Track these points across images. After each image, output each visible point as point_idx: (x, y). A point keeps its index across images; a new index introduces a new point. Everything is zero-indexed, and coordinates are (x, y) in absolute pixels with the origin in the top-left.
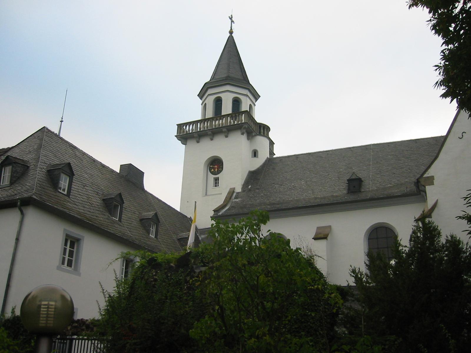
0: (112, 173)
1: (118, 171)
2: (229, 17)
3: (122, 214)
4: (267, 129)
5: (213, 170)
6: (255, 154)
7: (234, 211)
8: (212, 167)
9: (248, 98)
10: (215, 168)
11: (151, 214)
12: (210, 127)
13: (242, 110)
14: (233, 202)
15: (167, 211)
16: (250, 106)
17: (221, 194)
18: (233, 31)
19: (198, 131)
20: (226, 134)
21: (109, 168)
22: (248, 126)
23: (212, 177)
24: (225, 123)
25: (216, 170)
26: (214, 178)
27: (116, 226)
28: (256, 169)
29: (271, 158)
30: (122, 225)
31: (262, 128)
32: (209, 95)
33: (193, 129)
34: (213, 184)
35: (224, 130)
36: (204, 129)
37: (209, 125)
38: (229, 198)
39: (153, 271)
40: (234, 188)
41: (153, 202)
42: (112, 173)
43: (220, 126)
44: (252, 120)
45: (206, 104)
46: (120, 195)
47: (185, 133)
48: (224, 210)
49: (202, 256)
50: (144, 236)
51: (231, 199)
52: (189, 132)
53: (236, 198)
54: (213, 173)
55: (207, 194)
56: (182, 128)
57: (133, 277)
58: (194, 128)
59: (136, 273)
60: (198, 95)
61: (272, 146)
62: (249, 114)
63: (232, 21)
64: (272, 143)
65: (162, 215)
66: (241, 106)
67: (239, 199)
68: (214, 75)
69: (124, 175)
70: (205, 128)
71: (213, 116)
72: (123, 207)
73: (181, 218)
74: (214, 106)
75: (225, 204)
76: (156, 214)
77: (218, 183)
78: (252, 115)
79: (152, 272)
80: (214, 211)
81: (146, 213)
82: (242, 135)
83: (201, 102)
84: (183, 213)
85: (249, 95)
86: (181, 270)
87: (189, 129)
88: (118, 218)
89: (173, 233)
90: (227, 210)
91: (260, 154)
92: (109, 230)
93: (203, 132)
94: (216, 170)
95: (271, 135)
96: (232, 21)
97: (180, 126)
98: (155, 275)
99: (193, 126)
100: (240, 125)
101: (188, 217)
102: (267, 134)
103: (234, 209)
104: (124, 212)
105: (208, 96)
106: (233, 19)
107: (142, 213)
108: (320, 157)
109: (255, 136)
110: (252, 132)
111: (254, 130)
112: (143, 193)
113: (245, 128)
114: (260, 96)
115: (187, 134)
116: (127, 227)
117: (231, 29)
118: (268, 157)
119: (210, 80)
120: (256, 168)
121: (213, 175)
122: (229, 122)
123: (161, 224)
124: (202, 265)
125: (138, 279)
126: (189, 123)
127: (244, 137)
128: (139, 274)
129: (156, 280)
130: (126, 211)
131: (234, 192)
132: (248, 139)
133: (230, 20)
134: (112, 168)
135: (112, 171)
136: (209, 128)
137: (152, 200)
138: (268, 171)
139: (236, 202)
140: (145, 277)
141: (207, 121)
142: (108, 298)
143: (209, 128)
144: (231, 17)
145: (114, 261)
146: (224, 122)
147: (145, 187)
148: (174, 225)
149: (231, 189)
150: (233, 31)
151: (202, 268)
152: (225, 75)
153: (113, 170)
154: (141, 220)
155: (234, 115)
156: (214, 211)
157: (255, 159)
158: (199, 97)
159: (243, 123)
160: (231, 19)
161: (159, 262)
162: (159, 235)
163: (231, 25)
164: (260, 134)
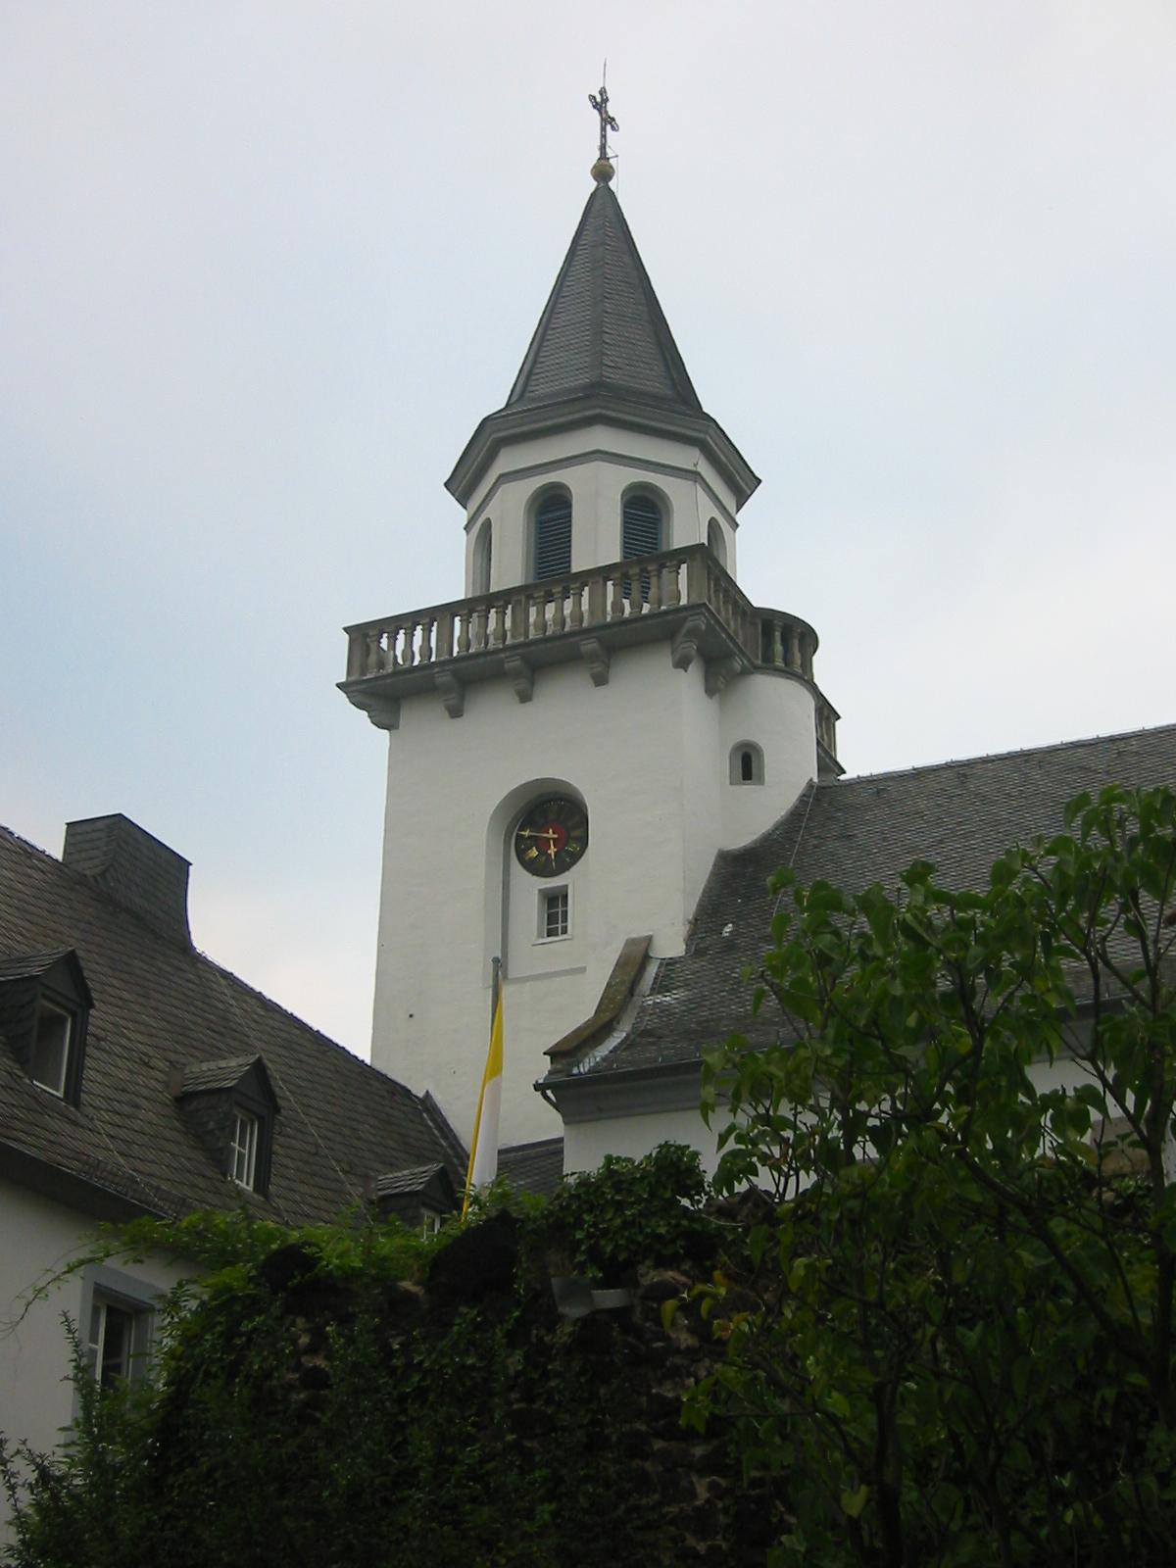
0: (28, 862)
1: (55, 848)
2: (592, 98)
3: (83, 1054)
4: (802, 637)
5: (534, 853)
6: (747, 764)
7: (651, 1056)
8: (530, 837)
9: (699, 488)
10: (548, 839)
11: (232, 1067)
12: (513, 637)
13: (676, 547)
14: (643, 1009)
15: (311, 1061)
16: (713, 526)
17: (583, 970)
18: (615, 166)
19: (455, 654)
20: (598, 668)
21: (8, 836)
22: (708, 624)
23: (529, 888)
24: (591, 611)
25: (552, 851)
26: (540, 890)
27: (55, 1124)
28: (755, 842)
29: (824, 784)
30: (83, 1121)
31: (778, 635)
32: (504, 478)
33: (431, 649)
34: (540, 917)
35: (589, 646)
36: (486, 644)
37: (508, 624)
38: (624, 989)
39: (293, 1324)
40: (649, 940)
41: (237, 1011)
42: (28, 862)
43: (567, 629)
44: (726, 591)
45: (487, 525)
46: (71, 961)
47: (390, 669)
48: (600, 1048)
49: (595, 1225)
50: (201, 1182)
51: (637, 992)
52: (407, 665)
53: (661, 987)
54: (536, 868)
55: (509, 977)
56: (373, 646)
57: (178, 1369)
58: (433, 644)
59: (190, 1339)
60: (446, 485)
61: (828, 730)
62: (709, 559)
63: (608, 121)
64: (826, 715)
65: (284, 1081)
66: (668, 535)
67: (680, 994)
68: (528, 378)
69: (88, 872)
70: (492, 640)
71: (526, 578)
72: (85, 1033)
73: (383, 1097)
74: (533, 530)
75: (606, 1017)
76: (259, 1067)
77: (565, 920)
78: (721, 562)
79: (288, 1330)
80: (554, 1054)
81: (204, 1066)
82: (682, 671)
83: (463, 516)
84: (391, 1075)
85: (703, 474)
86: (468, 1313)
87: (408, 649)
88: (62, 1089)
89: (342, 1170)
90: (616, 1048)
91: (772, 764)
92: (14, 1145)
93: (481, 660)
94: (552, 851)
95: (824, 668)
96: (608, 121)
97: (363, 637)
98: (311, 1350)
99: (427, 632)
100: (670, 617)
101: (414, 1092)
102: (802, 666)
103: (653, 1043)
104: (91, 1057)
105: (497, 481)
106: (612, 110)
107: (184, 1065)
108: (1082, 768)
109: (746, 672)
110: (730, 656)
111: (736, 644)
112: (185, 966)
113: (694, 633)
114: (759, 481)
115: (398, 672)
116: (112, 1131)
117: (603, 156)
118: (811, 780)
119: (507, 405)
120: (755, 837)
121: (535, 878)
122: (613, 603)
123: (282, 1124)
124: (594, 1278)
125: (207, 1373)
126: (407, 621)
127: (689, 684)
128: (213, 1346)
129: (315, 1380)
130: (105, 1050)
131: (646, 958)
132: (710, 690)
133: (596, 112)
134: (24, 837)
135: (28, 852)
136: (509, 641)
137: (232, 1002)
138: (815, 847)
139: (664, 1010)
140: (251, 1364)
141: (501, 603)
142: (31, 1487)
143: (509, 641)
144: (599, 99)
145: (58, 1278)
146: (585, 607)
147: (193, 937)
148: (346, 1131)
149: (631, 943)
150: (611, 167)
151: (595, 1292)
152: (584, 379)
153: (32, 847)
154: (182, 1100)
155: (634, 571)
156: (554, 1054)
157: (748, 788)
158: (453, 494)
159: (685, 608)
160: (599, 111)
161: (330, 1274)
162: (273, 1179)
163: (604, 136)
164: (767, 666)
